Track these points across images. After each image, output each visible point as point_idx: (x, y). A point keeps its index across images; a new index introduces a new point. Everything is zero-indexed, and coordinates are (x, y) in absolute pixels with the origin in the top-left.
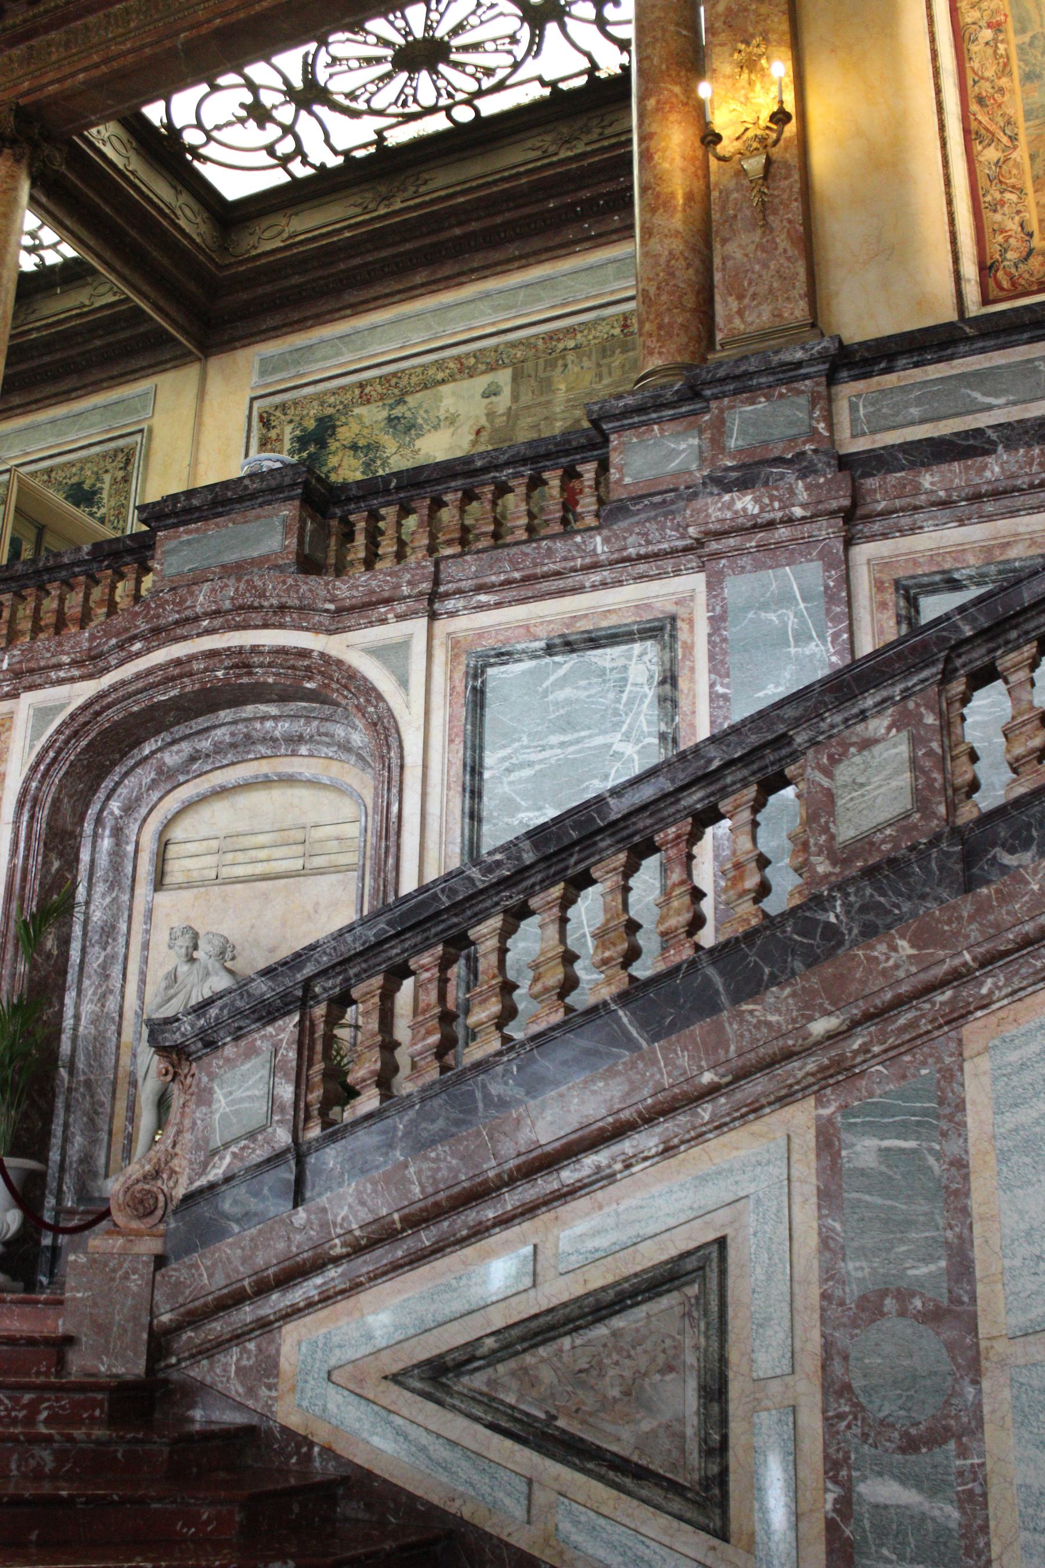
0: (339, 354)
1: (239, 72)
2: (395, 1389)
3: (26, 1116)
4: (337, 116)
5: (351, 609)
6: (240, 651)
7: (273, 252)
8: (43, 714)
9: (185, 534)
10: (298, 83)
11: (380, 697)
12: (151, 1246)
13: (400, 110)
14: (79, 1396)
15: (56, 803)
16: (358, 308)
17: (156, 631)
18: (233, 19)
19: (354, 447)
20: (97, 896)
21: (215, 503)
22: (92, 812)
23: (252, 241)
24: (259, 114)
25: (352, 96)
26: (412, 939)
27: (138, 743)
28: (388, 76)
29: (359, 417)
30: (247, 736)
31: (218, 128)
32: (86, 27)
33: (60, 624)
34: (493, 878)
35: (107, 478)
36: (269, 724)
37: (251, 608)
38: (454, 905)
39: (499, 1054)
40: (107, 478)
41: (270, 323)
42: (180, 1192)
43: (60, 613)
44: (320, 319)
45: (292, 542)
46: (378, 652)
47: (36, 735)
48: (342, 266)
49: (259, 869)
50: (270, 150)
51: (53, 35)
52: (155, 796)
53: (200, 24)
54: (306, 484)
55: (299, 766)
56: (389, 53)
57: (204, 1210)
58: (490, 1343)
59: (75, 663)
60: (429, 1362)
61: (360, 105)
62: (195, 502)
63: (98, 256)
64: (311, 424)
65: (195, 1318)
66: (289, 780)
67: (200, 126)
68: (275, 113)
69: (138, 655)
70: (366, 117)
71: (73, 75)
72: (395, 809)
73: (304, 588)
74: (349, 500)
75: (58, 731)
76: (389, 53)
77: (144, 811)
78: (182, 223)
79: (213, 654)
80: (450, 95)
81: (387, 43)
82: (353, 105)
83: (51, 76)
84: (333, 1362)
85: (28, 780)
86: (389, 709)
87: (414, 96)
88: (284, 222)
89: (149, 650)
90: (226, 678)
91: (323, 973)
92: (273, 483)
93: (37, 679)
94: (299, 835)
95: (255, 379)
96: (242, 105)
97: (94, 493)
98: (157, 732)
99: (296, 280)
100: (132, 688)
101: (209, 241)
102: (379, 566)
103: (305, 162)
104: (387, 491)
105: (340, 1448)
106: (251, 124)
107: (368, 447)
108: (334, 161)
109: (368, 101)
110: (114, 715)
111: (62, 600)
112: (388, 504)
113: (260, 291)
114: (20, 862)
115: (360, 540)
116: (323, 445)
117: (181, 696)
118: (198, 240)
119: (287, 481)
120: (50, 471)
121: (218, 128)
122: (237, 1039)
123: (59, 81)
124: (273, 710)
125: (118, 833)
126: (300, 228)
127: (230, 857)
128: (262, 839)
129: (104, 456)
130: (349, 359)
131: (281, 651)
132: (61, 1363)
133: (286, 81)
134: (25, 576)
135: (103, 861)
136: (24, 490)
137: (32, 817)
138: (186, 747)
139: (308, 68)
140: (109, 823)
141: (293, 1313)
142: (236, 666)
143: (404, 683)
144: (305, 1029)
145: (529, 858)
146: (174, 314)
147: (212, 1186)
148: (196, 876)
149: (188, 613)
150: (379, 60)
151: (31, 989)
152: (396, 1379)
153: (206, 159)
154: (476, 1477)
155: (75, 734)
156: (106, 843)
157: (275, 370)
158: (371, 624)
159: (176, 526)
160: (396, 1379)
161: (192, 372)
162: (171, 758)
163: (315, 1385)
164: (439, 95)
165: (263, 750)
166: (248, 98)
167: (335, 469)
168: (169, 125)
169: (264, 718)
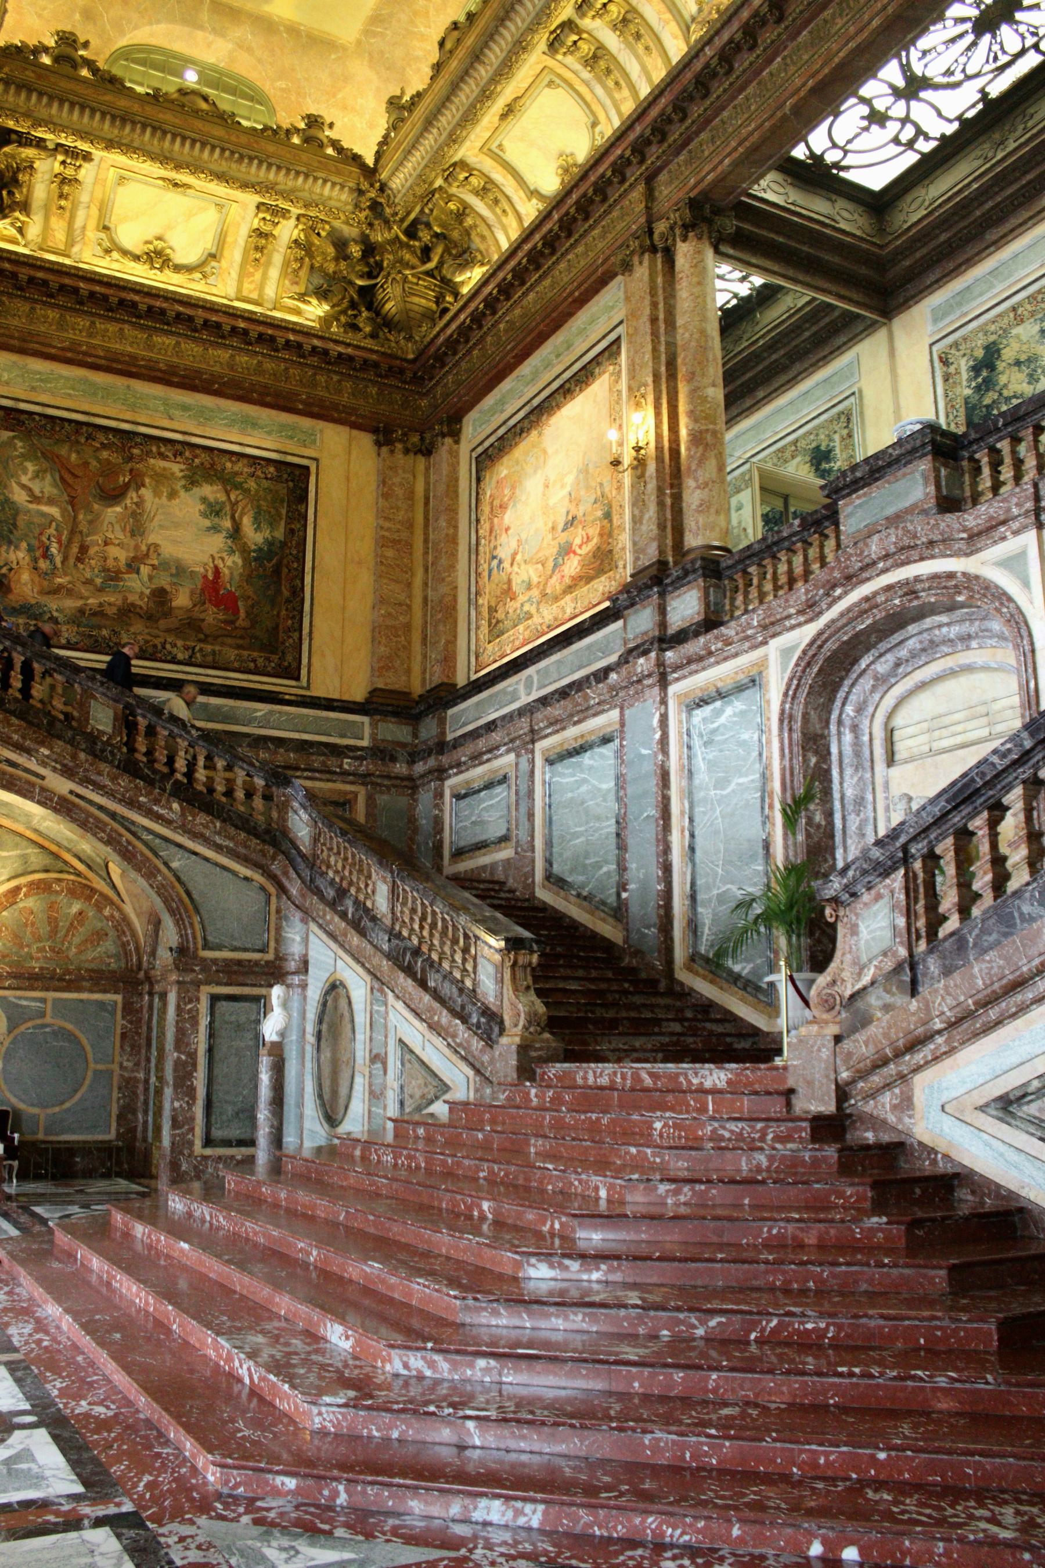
0: (992, 286)
1: (855, 94)
2: (982, 1115)
3: (819, 941)
4: (941, 93)
5: (979, 534)
6: (907, 582)
7: (920, 221)
8: (786, 652)
9: (857, 499)
10: (901, 83)
11: (1010, 599)
12: (834, 1029)
13: (993, 66)
14: (790, 1124)
15: (805, 715)
16: (998, 243)
17: (848, 578)
18: (820, 77)
19: (1018, 363)
20: (847, 778)
21: (872, 472)
22: (834, 717)
23: (902, 217)
24: (877, 118)
25: (949, 73)
26: (966, 810)
27: (856, 661)
28: (974, 44)
29: (1017, 336)
30: (931, 641)
31: (849, 142)
32: (723, 122)
33: (792, 582)
34: (1006, 761)
35: (837, 437)
36: (945, 630)
37: (910, 547)
38: (986, 784)
39: (1028, 884)
40: (837, 437)
41: (932, 278)
42: (848, 993)
43: (790, 572)
44: (970, 262)
45: (931, 489)
46: (1008, 563)
47: (784, 670)
48: (978, 213)
49: (959, 740)
50: (896, 141)
51: (703, 136)
52: (877, 696)
53: (799, 89)
54: (933, 442)
55: (974, 656)
56: (968, 26)
57: (860, 1004)
58: (1036, 1084)
59: (800, 612)
60: (1000, 1098)
61: (959, 76)
62: (858, 474)
63: (784, 277)
64: (980, 353)
65: (863, 1075)
66: (968, 669)
67: (835, 146)
68: (890, 113)
69: (840, 598)
70: (966, 84)
71: (721, 162)
72: (1032, 685)
73: (943, 525)
74: (971, 443)
75: (797, 665)
76: (968, 26)
77: (871, 709)
78: (842, 225)
79: (889, 588)
80: (1033, 34)
81: (963, 20)
82: (952, 79)
83: (707, 168)
84: (944, 1099)
85: (783, 703)
86: (1018, 608)
87: (1002, 48)
88: (923, 192)
89: (846, 593)
90: (902, 604)
91: (914, 839)
92: (909, 447)
93: (777, 628)
94: (982, 709)
95: (930, 328)
96: (863, 118)
97: (830, 451)
98: (868, 650)
99: (943, 237)
100: (839, 624)
101: (869, 231)
102: (1002, 490)
103: (927, 138)
104: (998, 430)
105: (954, 1155)
106: (875, 128)
107: (1029, 360)
108: (951, 129)
109: (963, 71)
110: (831, 646)
111: (790, 563)
112: (1001, 439)
113: (918, 255)
114: (787, 764)
115: (986, 471)
116: (992, 367)
117: (875, 623)
118: (858, 233)
119: (918, 443)
120: (795, 442)
121: (849, 142)
122: (869, 889)
123: (714, 169)
124: (944, 618)
125: (855, 728)
126: (937, 194)
127: (937, 733)
128: (957, 717)
129: (831, 421)
130: (1000, 289)
131: (935, 577)
132: (789, 1105)
133: (892, 86)
134: (761, 551)
135: (848, 750)
136: (763, 475)
137: (790, 730)
138: (890, 658)
139: (906, 69)
140: (847, 722)
141: (918, 1069)
142: (906, 594)
143: (1026, 584)
144: (910, 879)
145: (1028, 744)
146: (855, 296)
147: (865, 988)
148: (916, 751)
149: (867, 560)
150: (961, 36)
151: (809, 852)
152: (982, 1108)
153: (847, 168)
154: (1035, 1173)
155: (809, 664)
156: (848, 737)
157: (945, 314)
158: (995, 542)
159: (849, 495)
160: (982, 1108)
161: (881, 335)
162: (882, 667)
163: (935, 1114)
164: (1023, 38)
165: (946, 649)
166: (865, 110)
167: (1005, 386)
168: (812, 155)
169: (940, 626)
